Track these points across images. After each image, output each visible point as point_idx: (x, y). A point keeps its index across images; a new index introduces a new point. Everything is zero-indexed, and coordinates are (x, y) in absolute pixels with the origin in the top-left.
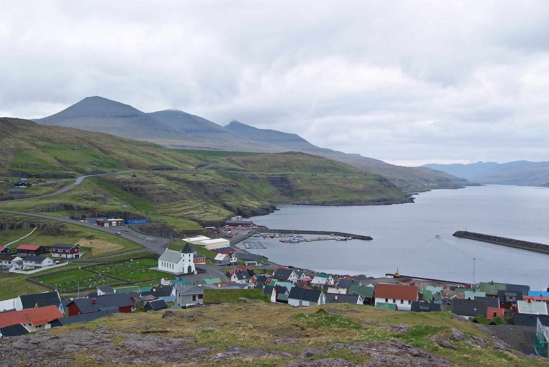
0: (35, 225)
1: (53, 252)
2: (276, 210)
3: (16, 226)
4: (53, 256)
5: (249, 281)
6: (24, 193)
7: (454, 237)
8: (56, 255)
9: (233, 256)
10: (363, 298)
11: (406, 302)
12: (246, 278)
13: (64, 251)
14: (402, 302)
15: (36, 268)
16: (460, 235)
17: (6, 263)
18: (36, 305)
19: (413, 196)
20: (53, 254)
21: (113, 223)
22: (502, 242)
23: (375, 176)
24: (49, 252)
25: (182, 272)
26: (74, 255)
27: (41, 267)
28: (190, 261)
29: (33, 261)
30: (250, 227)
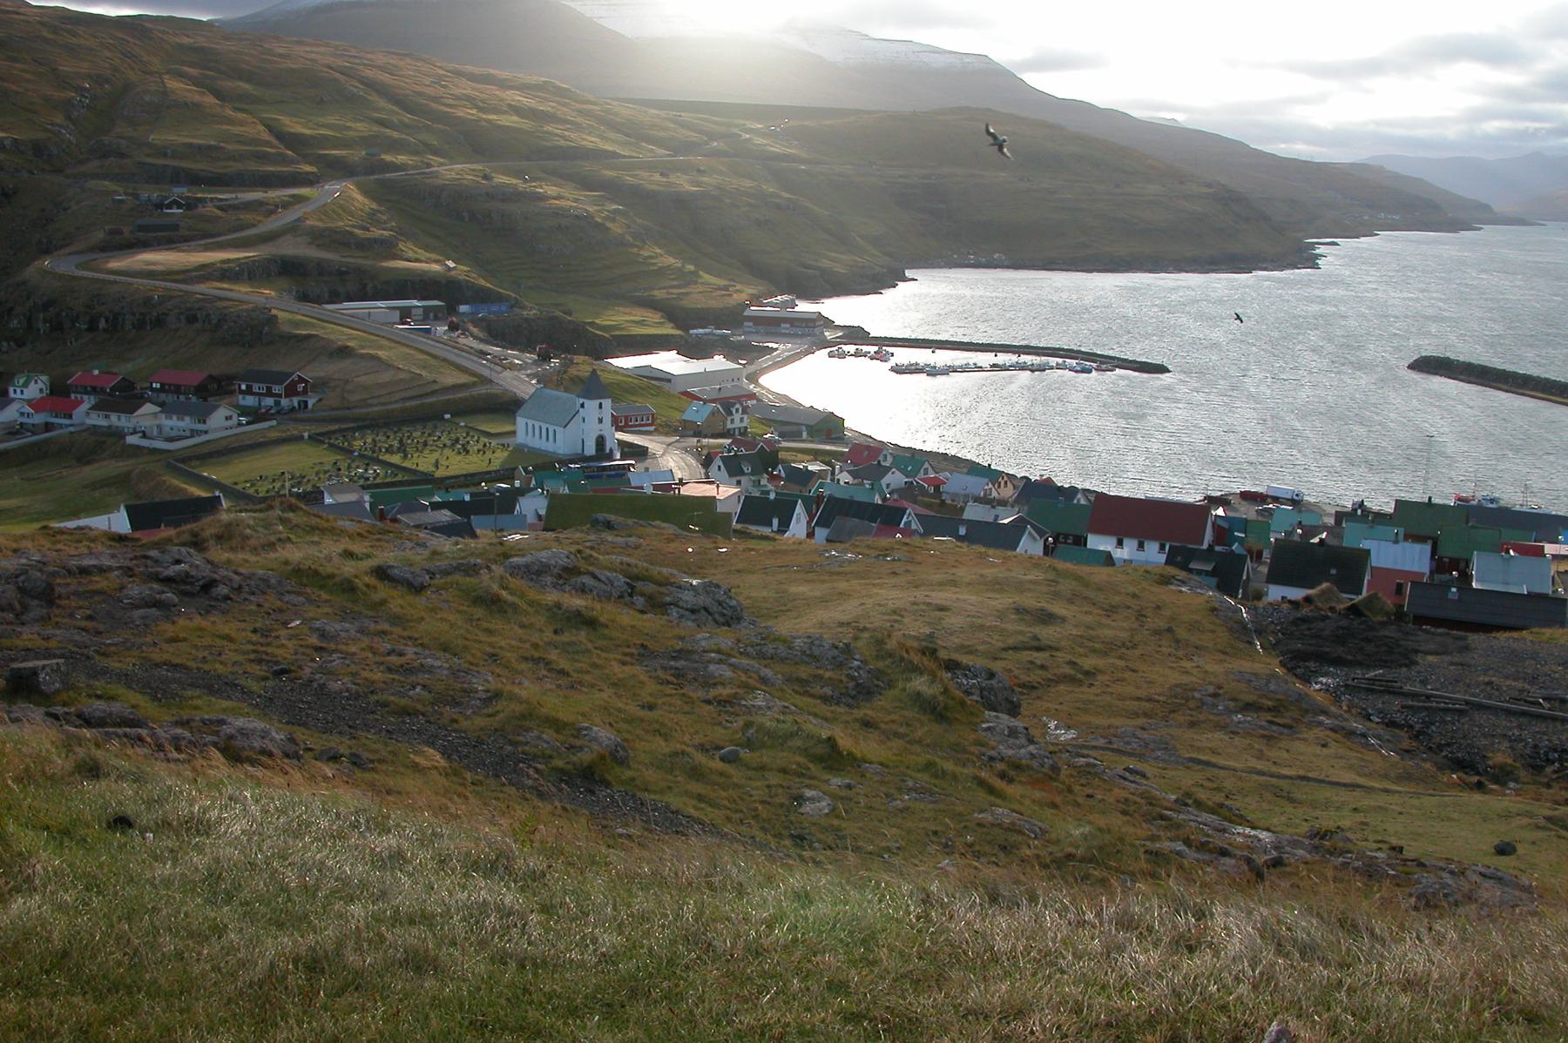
0: (199, 316)
1: (242, 392)
2: (906, 280)
3: (150, 319)
4: (242, 402)
5: (759, 481)
6: (176, 227)
7: (1410, 371)
8: (250, 401)
9: (737, 410)
10: (1041, 533)
11: (1152, 548)
12: (752, 474)
13: (269, 389)
14: (1141, 546)
15: (194, 433)
16: (1429, 365)
17: (119, 419)
18: (163, 525)
19: (1321, 250)
20: (241, 397)
21: (414, 311)
22: (1543, 391)
23: (1209, 186)
24: (232, 392)
25: (580, 452)
26: (295, 401)
27: (206, 432)
28: (600, 421)
29: (187, 415)
30: (814, 327)
